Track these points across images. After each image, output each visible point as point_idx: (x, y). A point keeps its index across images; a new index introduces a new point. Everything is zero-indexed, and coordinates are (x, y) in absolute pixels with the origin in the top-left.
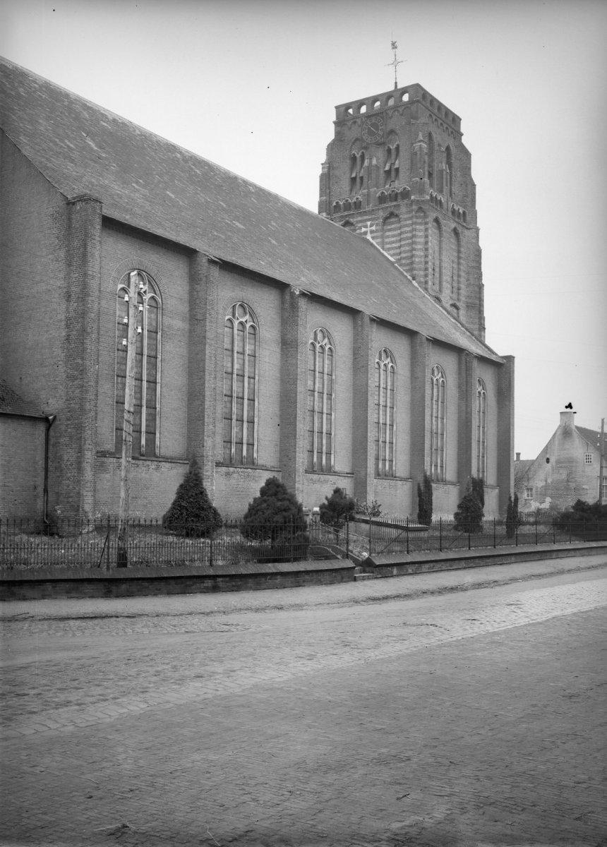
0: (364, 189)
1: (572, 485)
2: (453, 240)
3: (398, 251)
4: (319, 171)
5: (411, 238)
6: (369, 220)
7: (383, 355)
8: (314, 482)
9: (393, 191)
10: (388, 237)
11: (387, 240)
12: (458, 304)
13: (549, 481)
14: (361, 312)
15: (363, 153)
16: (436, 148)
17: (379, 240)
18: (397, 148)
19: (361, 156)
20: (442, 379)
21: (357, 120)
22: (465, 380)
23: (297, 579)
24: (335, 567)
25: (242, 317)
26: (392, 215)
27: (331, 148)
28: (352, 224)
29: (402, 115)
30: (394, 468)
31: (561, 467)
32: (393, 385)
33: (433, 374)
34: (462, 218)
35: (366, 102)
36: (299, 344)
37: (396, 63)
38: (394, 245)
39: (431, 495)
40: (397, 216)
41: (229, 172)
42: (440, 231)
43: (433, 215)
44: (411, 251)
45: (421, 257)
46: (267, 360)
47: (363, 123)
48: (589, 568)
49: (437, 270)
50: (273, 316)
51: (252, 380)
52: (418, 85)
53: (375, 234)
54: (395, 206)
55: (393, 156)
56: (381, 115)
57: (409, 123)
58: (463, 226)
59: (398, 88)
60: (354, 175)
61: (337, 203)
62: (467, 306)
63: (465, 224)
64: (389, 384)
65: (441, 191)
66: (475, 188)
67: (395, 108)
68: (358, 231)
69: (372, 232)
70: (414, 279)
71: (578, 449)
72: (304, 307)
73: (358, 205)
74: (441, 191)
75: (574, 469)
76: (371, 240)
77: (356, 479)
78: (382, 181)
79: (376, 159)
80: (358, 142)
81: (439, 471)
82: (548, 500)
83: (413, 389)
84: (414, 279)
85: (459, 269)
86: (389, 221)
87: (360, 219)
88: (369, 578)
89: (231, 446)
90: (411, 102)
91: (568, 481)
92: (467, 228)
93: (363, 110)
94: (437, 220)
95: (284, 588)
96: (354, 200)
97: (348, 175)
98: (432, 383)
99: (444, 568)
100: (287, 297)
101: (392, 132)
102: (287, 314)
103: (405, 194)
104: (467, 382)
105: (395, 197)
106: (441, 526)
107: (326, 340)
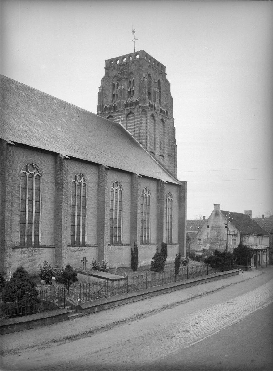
0: (118, 100)
1: (219, 238)
2: (161, 124)
3: (134, 130)
4: (97, 91)
5: (139, 124)
6: (120, 115)
7: (115, 185)
8: (74, 251)
9: (131, 101)
10: (129, 123)
11: (128, 125)
12: (163, 155)
13: (209, 236)
14: (101, 165)
15: (118, 83)
16: (153, 80)
17: (125, 125)
18: (134, 81)
19: (117, 84)
20: (148, 194)
21: (115, 67)
22: (160, 194)
23: (29, 325)
24: (54, 315)
25: (31, 171)
26: (131, 113)
27: (104, 80)
28: (112, 117)
29: (135, 65)
30: (121, 240)
31: (214, 230)
32: (121, 199)
33: (143, 192)
34: (166, 114)
35: (119, 58)
36: (64, 183)
37: (134, 40)
38: (132, 127)
39: (137, 254)
40: (133, 113)
41: (44, 93)
42: (154, 121)
43: (150, 113)
44: (139, 130)
45: (144, 133)
46: (47, 191)
47: (118, 68)
48: (212, 292)
49: (153, 139)
50: (51, 169)
51: (38, 203)
52: (143, 51)
53: (123, 122)
54: (132, 108)
55: (132, 85)
56: (126, 65)
57: (139, 69)
58: (166, 118)
59: (136, 51)
60: (114, 93)
61: (106, 106)
62: (168, 156)
63: (167, 117)
64: (119, 198)
65: (155, 101)
66: (172, 100)
67: (133, 62)
68: (115, 120)
69: (122, 121)
70: (141, 143)
71: (222, 222)
72: (67, 164)
73: (115, 108)
74: (155, 101)
75: (220, 231)
76: (121, 124)
77: (99, 247)
78: (126, 97)
79: (124, 86)
80: (116, 77)
81: (147, 239)
82: (208, 245)
83: (132, 201)
84: (141, 143)
85: (164, 138)
86: (129, 115)
87: (116, 114)
88: (78, 317)
89: (25, 237)
90: (140, 59)
91: (217, 236)
92: (168, 119)
93: (118, 62)
94: (152, 115)
95: (20, 331)
96: (114, 105)
97: (111, 93)
98: (143, 197)
99: (129, 302)
100: (58, 160)
101: (131, 73)
102: (58, 168)
103: (137, 103)
104: (161, 195)
105: (131, 104)
106: (143, 268)
107: (82, 180)
